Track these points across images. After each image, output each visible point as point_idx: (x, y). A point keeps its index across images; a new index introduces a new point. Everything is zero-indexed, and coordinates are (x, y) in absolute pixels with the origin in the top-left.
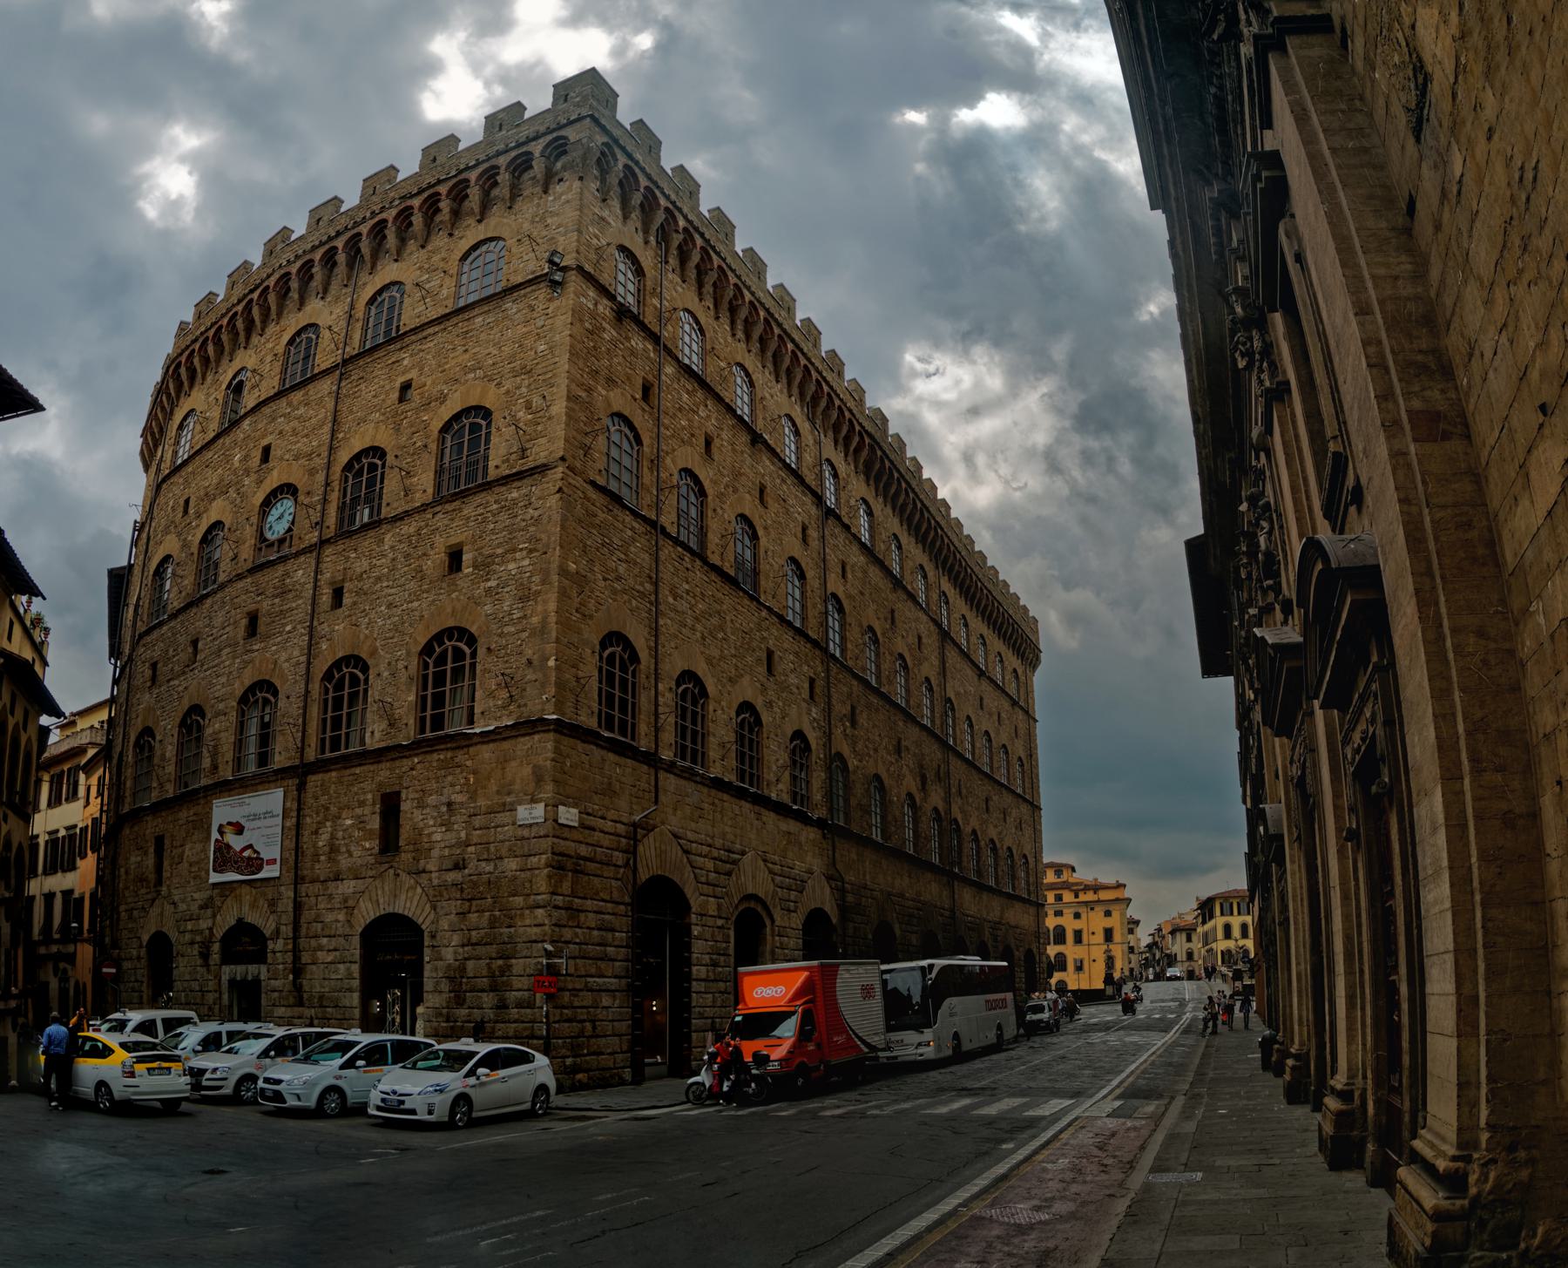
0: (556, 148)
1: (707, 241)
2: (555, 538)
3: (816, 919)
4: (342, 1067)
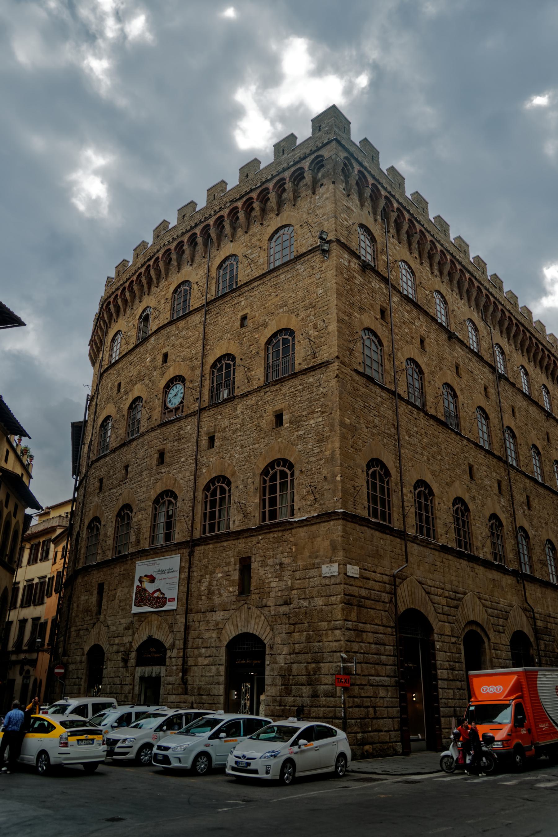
0: (317, 163)
1: (412, 215)
2: (336, 405)
3: (518, 639)
4: (210, 738)
